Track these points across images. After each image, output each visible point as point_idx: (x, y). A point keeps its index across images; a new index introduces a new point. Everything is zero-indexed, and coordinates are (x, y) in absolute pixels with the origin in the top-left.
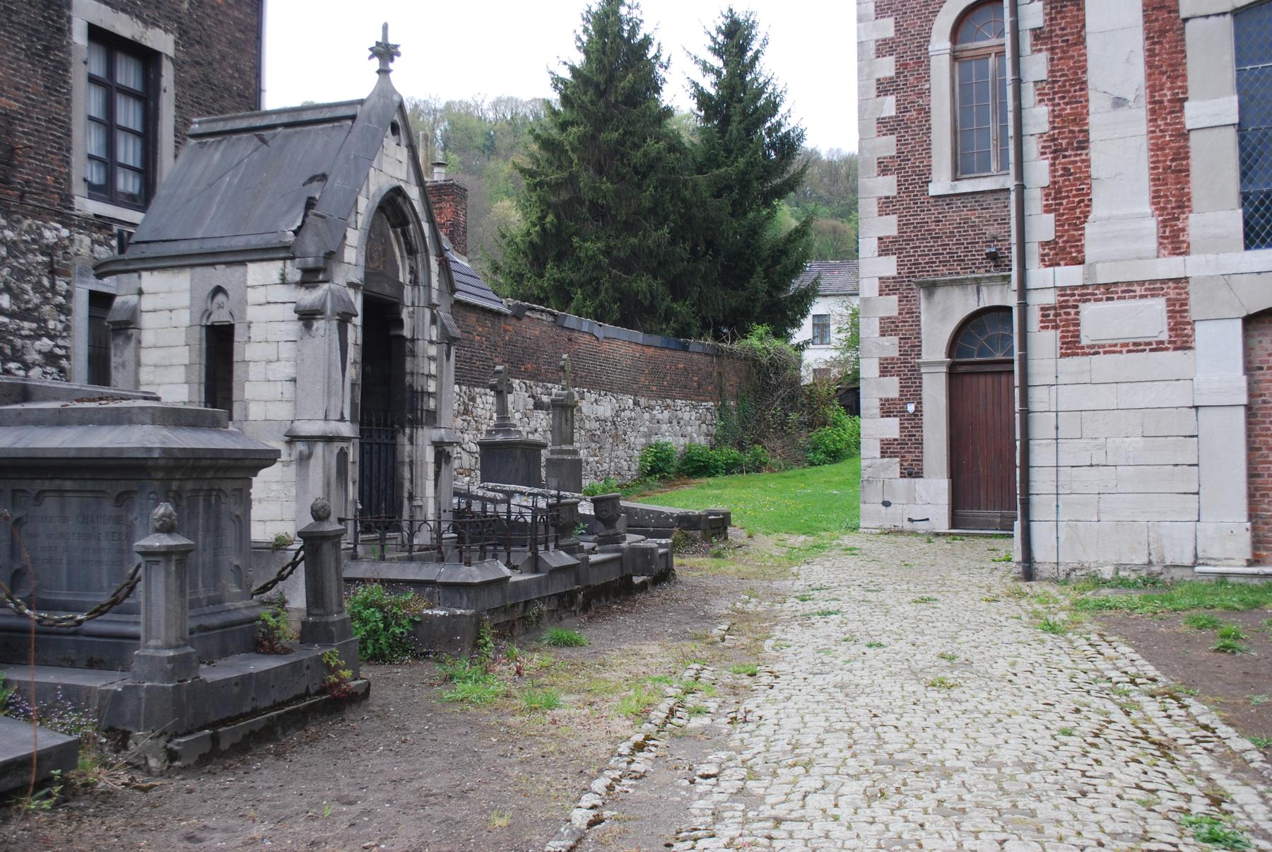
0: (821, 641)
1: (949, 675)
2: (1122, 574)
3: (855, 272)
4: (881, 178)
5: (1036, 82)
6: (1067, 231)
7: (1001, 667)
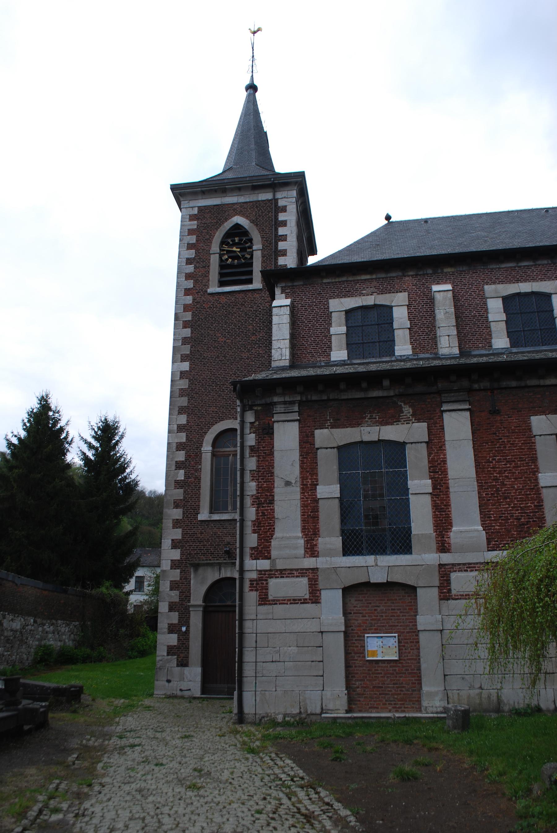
0: (130, 763)
1: (199, 781)
2: (287, 719)
3: (159, 555)
4: (175, 510)
5: (250, 471)
6: (263, 543)
7: (226, 775)
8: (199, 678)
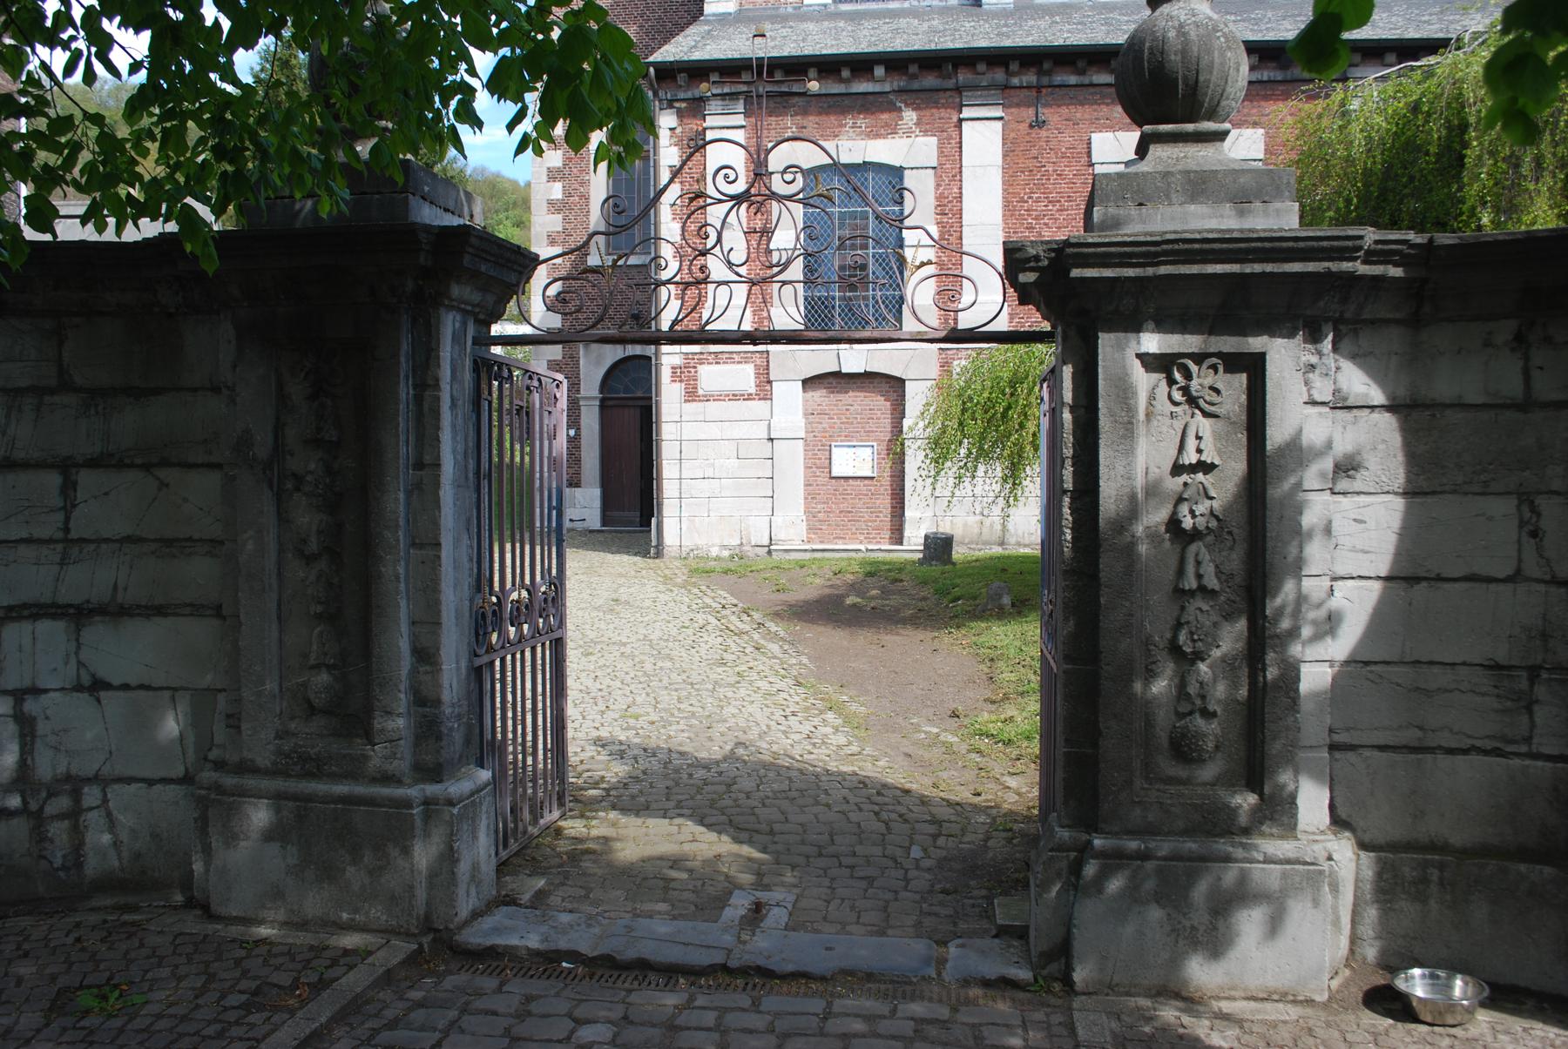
8: (597, 503)
